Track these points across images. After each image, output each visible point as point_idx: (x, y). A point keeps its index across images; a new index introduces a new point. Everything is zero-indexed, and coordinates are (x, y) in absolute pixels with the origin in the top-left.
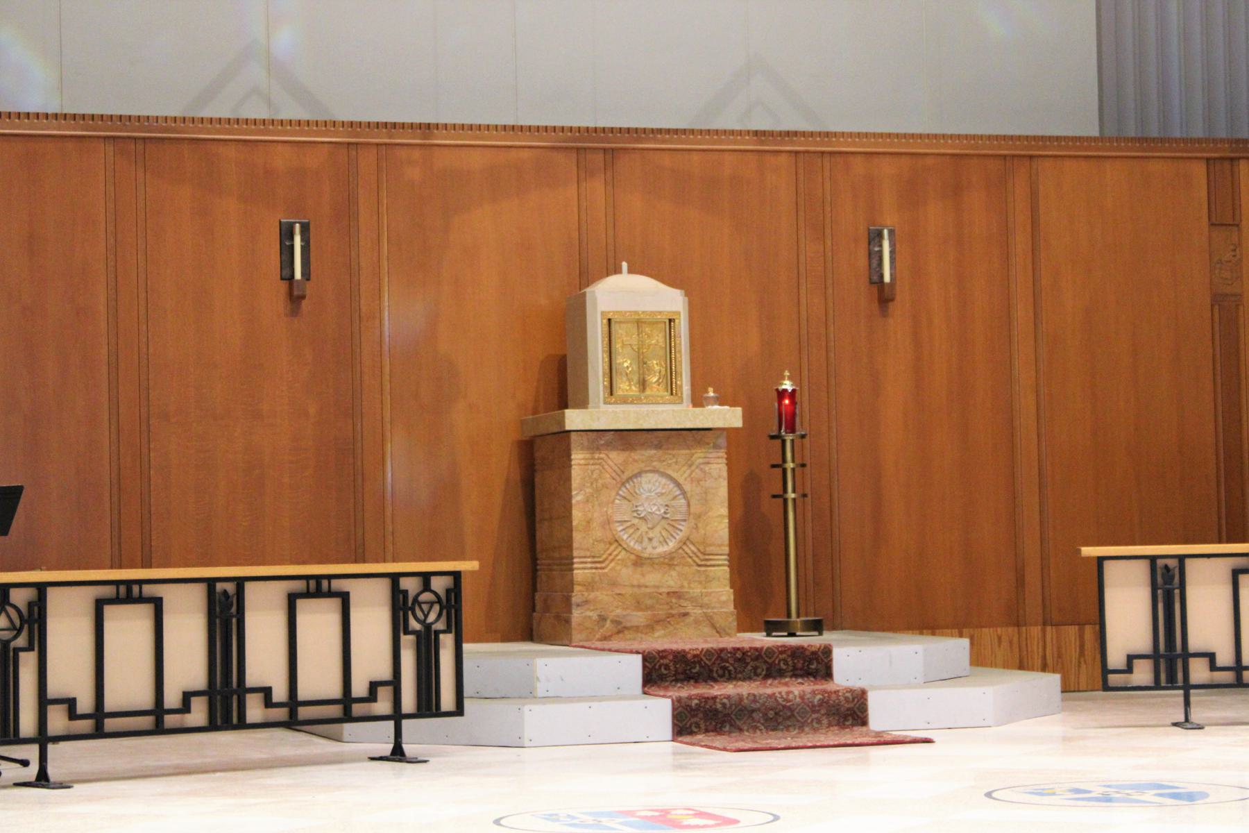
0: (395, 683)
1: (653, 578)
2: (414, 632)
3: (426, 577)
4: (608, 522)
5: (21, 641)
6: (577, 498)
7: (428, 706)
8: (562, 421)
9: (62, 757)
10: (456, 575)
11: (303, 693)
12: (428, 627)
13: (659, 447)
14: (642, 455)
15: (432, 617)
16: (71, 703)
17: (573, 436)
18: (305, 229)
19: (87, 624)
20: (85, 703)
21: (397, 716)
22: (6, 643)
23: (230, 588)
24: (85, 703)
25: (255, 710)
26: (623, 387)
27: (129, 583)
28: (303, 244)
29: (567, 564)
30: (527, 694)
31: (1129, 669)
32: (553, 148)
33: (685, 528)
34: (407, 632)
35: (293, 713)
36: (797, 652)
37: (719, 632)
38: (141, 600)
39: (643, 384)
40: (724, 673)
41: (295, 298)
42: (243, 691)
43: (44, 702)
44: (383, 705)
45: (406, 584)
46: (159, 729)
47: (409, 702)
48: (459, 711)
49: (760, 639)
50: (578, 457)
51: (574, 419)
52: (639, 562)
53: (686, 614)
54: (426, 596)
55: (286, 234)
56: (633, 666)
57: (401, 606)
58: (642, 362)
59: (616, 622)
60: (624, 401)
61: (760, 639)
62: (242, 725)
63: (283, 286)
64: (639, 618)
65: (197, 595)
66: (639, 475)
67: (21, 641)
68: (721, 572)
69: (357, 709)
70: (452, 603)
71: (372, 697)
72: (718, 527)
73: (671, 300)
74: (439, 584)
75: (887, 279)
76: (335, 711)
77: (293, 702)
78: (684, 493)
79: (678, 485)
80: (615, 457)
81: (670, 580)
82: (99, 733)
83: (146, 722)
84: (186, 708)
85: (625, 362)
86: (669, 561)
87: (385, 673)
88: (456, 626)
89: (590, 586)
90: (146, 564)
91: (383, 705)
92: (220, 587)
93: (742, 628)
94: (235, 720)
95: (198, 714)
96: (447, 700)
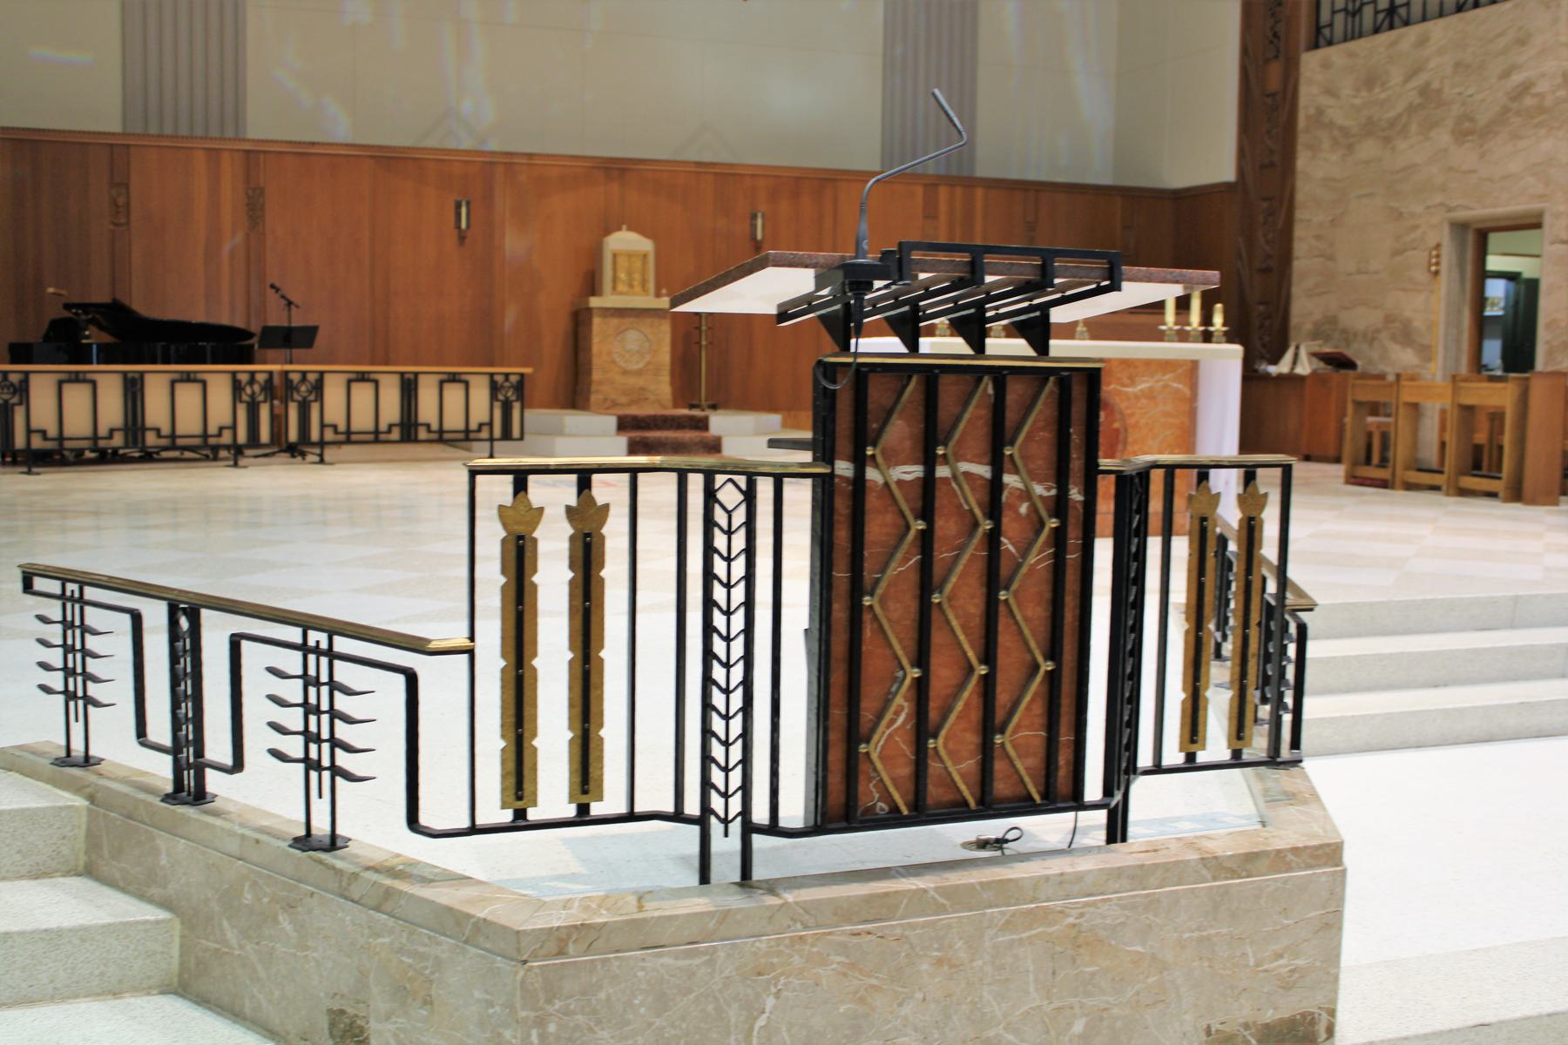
0: (491, 424)
1: (632, 381)
2: (501, 401)
3: (507, 375)
4: (610, 353)
5: (312, 397)
6: (596, 340)
7: (507, 435)
8: (587, 302)
9: (330, 453)
10: (522, 375)
11: (179, 431)
12: (507, 398)
13: (636, 316)
14: (628, 321)
15: (510, 394)
16: (335, 427)
17: (595, 311)
18: (468, 204)
19: (436, 392)
20: (435, 426)
21: (491, 440)
22: (6, 402)
23: (412, 377)
24: (435, 426)
25: (422, 434)
26: (621, 287)
27: (454, 374)
28: (1500, 437)
29: (589, 372)
30: (560, 432)
31: (220, 435)
32: (593, 167)
33: (648, 358)
34: (241, 401)
35: (441, 437)
36: (692, 418)
37: (664, 407)
38: (195, 381)
39: (631, 286)
40: (342, 433)
41: (462, 238)
42: (144, 429)
43: (323, 426)
44: (485, 434)
45: (499, 379)
46: (377, 441)
47: (497, 432)
48: (521, 438)
49: (685, 412)
50: (597, 321)
51: (595, 302)
52: (625, 372)
53: (646, 399)
54: (507, 384)
55: (458, 206)
56: (611, 421)
57: (494, 388)
58: (630, 273)
59: (613, 401)
60: (621, 293)
61: (685, 412)
62: (416, 441)
63: (456, 232)
64: (623, 400)
65: (396, 380)
66: (626, 330)
67: (312, 397)
68: (665, 378)
69: (382, 437)
70: (520, 387)
71: (479, 430)
72: (665, 356)
73: (645, 245)
74: (514, 379)
75: (759, 236)
76: (461, 436)
77: (348, 432)
78: (648, 340)
79: (645, 335)
80: (615, 322)
81: (640, 382)
82: (348, 442)
83: (371, 437)
84: (389, 431)
85: (622, 275)
86: (639, 373)
87: (227, 421)
88: (521, 397)
89: (601, 383)
90: (372, 363)
91: (485, 434)
92: (407, 376)
93: (676, 406)
94: (413, 437)
95: (395, 435)
96: (516, 432)
